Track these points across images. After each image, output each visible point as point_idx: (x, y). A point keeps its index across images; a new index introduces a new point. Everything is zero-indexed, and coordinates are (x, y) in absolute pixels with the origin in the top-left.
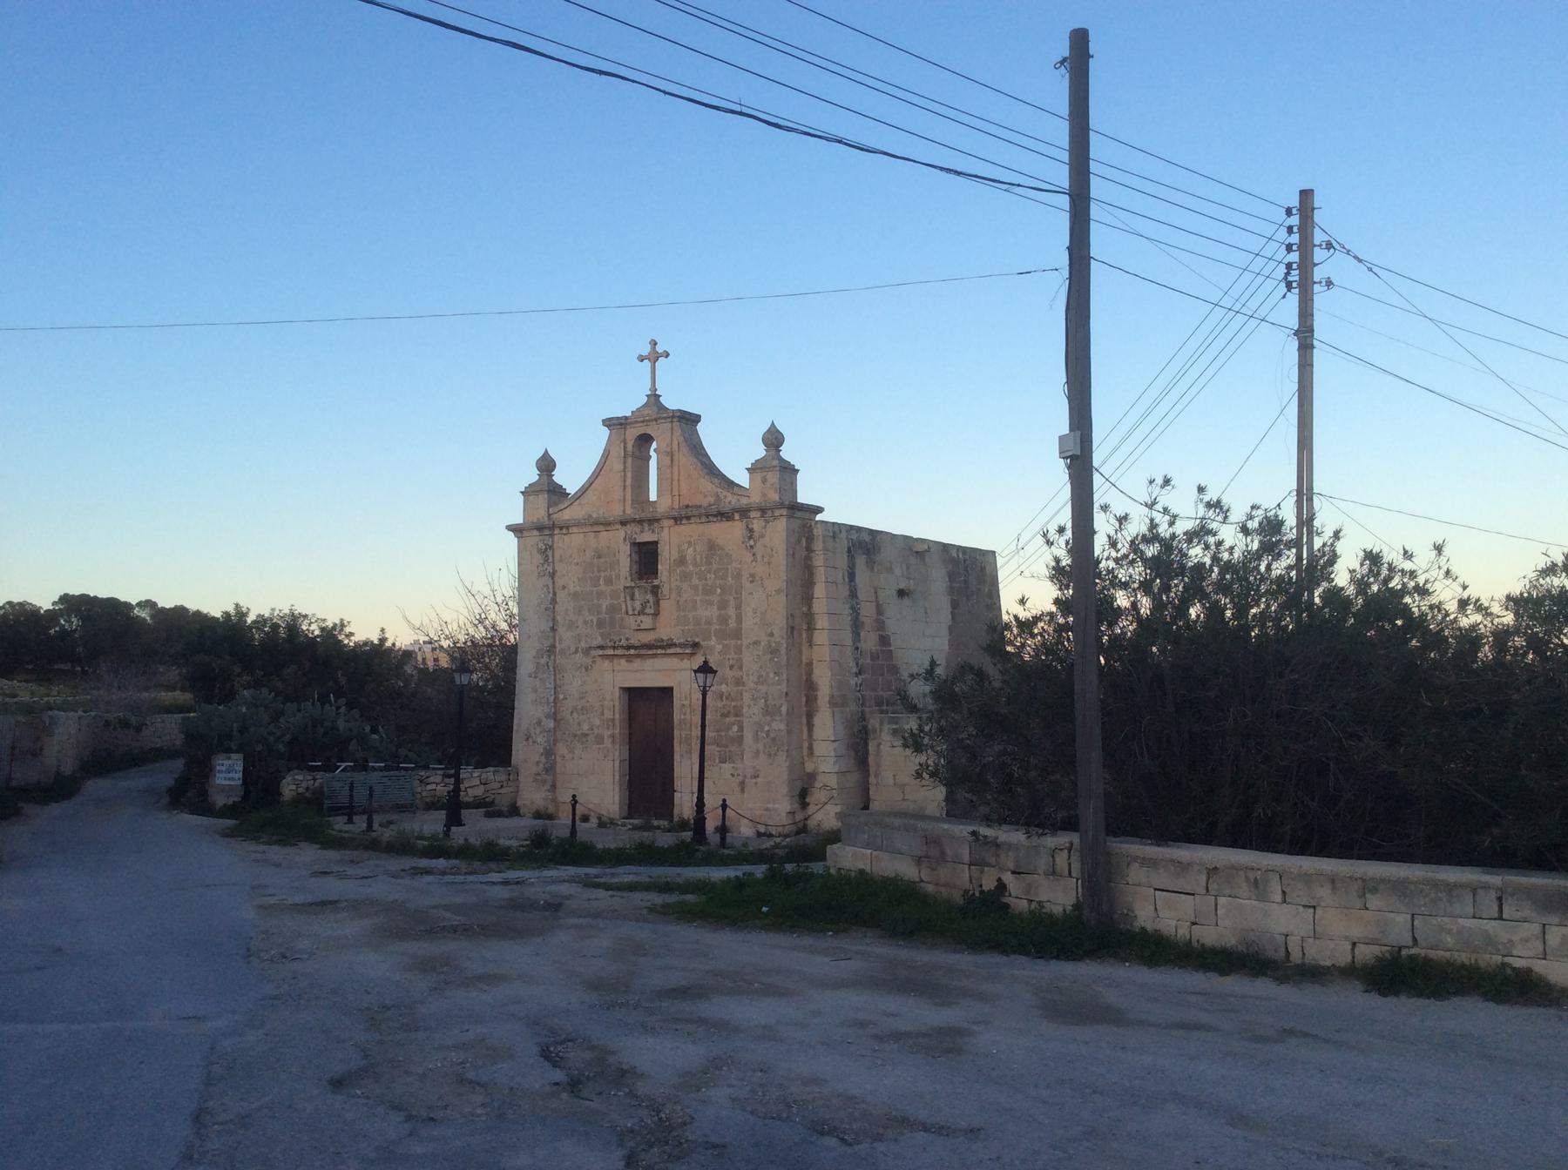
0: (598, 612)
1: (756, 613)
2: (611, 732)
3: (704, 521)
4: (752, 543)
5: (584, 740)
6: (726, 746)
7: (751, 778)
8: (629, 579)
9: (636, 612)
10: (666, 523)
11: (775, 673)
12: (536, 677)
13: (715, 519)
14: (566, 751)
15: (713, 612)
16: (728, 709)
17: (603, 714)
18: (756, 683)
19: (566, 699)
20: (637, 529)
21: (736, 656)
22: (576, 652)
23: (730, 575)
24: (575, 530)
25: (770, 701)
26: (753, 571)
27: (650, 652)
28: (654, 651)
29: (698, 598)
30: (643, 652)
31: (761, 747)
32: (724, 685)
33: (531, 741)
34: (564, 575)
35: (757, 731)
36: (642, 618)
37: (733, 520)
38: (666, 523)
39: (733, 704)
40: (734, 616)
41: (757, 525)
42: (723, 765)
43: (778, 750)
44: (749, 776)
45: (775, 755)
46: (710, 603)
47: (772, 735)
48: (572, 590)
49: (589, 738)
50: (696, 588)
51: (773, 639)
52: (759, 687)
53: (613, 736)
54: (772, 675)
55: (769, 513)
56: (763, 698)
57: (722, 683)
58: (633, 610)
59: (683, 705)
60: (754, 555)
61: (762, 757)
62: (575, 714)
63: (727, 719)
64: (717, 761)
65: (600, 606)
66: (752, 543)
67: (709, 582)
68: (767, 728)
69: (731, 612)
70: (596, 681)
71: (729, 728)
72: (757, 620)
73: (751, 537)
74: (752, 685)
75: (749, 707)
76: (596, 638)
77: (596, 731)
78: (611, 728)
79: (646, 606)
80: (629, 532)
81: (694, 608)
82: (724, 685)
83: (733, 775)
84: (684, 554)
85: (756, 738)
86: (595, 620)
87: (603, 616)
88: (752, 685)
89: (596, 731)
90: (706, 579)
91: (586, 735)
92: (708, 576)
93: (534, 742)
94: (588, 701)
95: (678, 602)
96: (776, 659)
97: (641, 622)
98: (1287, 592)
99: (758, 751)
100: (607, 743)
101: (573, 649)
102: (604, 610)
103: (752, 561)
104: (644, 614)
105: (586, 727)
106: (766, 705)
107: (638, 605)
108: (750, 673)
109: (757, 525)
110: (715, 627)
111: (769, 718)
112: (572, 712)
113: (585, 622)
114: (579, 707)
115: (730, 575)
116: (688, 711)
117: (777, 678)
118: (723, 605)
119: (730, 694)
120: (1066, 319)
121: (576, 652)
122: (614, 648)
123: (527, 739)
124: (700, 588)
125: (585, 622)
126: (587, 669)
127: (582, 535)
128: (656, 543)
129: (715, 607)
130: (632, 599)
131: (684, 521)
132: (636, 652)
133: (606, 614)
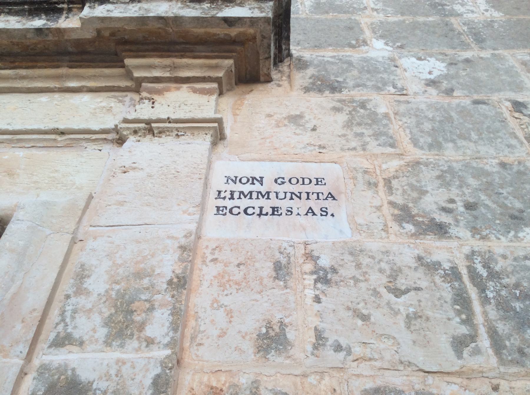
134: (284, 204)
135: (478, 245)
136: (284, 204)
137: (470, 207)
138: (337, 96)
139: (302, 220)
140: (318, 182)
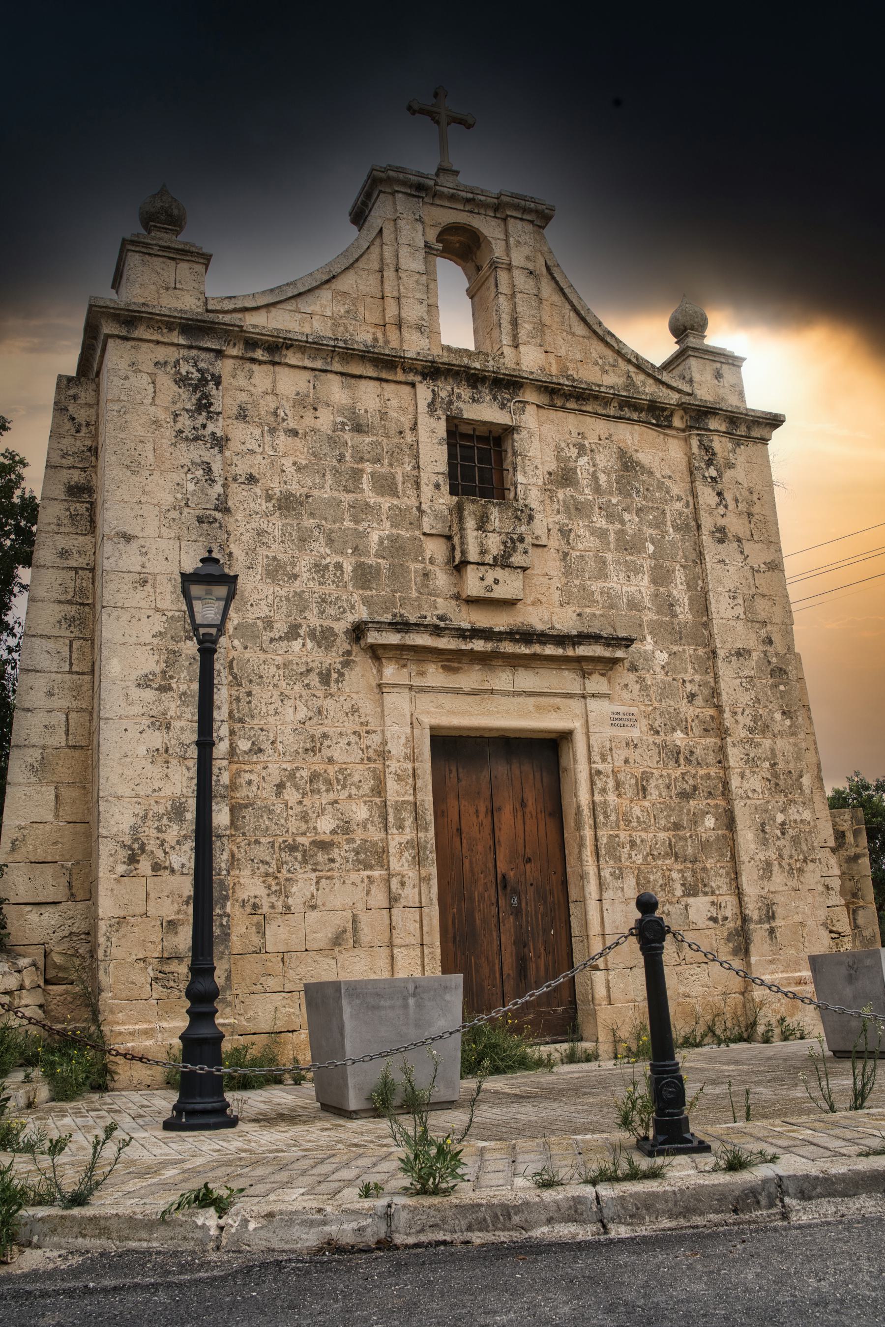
0: (356, 549)
1: (734, 598)
2: (409, 834)
3: (612, 413)
4: (712, 472)
5: (321, 857)
6: (695, 860)
7: (760, 922)
8: (445, 489)
9: (489, 559)
10: (530, 396)
11: (784, 713)
12: (165, 689)
13: (635, 416)
14: (261, 891)
15: (643, 586)
16: (691, 782)
17: (379, 789)
18: (751, 731)
19: (260, 750)
20: (465, 392)
21: (697, 678)
22: (293, 633)
23: (669, 523)
24: (292, 358)
25: (781, 766)
26: (721, 522)
27: (524, 650)
28: (537, 649)
29: (609, 556)
30: (508, 647)
31: (772, 854)
32: (679, 734)
33: (145, 866)
34: (251, 452)
35: (763, 824)
36: (499, 573)
37: (670, 427)
38: (530, 396)
39: (702, 772)
40: (686, 601)
41: (720, 445)
42: (691, 900)
43: (805, 861)
44: (755, 916)
45: (801, 870)
46: (637, 570)
47: (792, 833)
48: (277, 489)
49: (335, 853)
50: (602, 534)
51: (770, 649)
52: (758, 738)
53: (417, 846)
54: (778, 716)
55: (742, 431)
56: (768, 760)
57: (674, 730)
58: (483, 552)
59: (599, 773)
60: (719, 494)
61: (778, 878)
62: (291, 795)
63: (693, 803)
64: (679, 892)
65: (364, 535)
66: (712, 472)
67: (630, 529)
68: (780, 818)
69: (679, 591)
70: (355, 710)
71: (696, 819)
72: (740, 610)
73: (709, 463)
74: (744, 733)
75: (742, 775)
76: (353, 607)
77: (359, 835)
78: (409, 822)
79: (514, 549)
80: (443, 394)
81: (602, 574)
82: (679, 734)
83: (714, 919)
84: (572, 465)
85: (764, 840)
86: (348, 567)
87: (371, 561)
88: (744, 733)
89: (359, 835)
90: (623, 522)
91: (324, 846)
92: (627, 517)
93: (156, 867)
94: (331, 760)
95: (566, 555)
96: (782, 688)
97: (496, 582)
98: (704, 846)
99: (768, 864)
100: (400, 863)
101: (281, 627)
102: (374, 547)
103: (718, 505)
104: (504, 566)
105: (325, 825)
106: (775, 775)
107: (494, 544)
108: (740, 710)
109: (720, 445)
110: (649, 616)
111: (782, 799)
112: (280, 786)
113: (319, 569)
114: (305, 774)
115: (669, 523)
116: (611, 784)
117: (788, 722)
118: (661, 577)
119: (692, 753)
120: (473, 315)
121: (293, 633)
122: (436, 631)
123: (133, 859)
124: (612, 537)
125: (319, 569)
126: (325, 679)
127: (307, 375)
128: (509, 430)
129: (646, 577)
130: (482, 524)
131: (571, 405)
132: (489, 646)
133: (377, 555)
134: (626, 723)
135: (665, 738)
136: (626, 723)
137: (665, 725)
138: (637, 674)
139: (630, 728)
140: (633, 714)
